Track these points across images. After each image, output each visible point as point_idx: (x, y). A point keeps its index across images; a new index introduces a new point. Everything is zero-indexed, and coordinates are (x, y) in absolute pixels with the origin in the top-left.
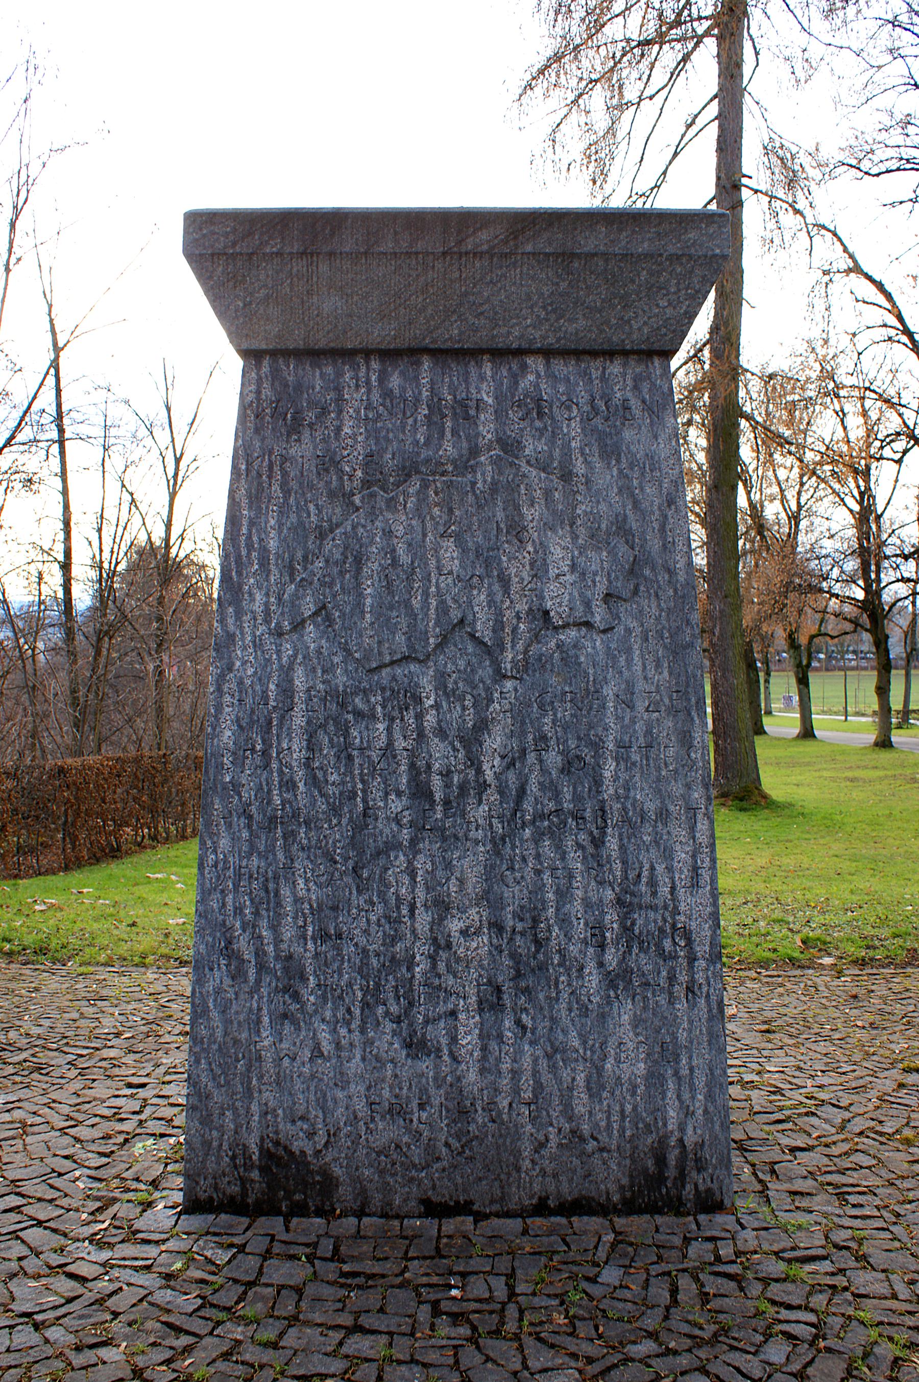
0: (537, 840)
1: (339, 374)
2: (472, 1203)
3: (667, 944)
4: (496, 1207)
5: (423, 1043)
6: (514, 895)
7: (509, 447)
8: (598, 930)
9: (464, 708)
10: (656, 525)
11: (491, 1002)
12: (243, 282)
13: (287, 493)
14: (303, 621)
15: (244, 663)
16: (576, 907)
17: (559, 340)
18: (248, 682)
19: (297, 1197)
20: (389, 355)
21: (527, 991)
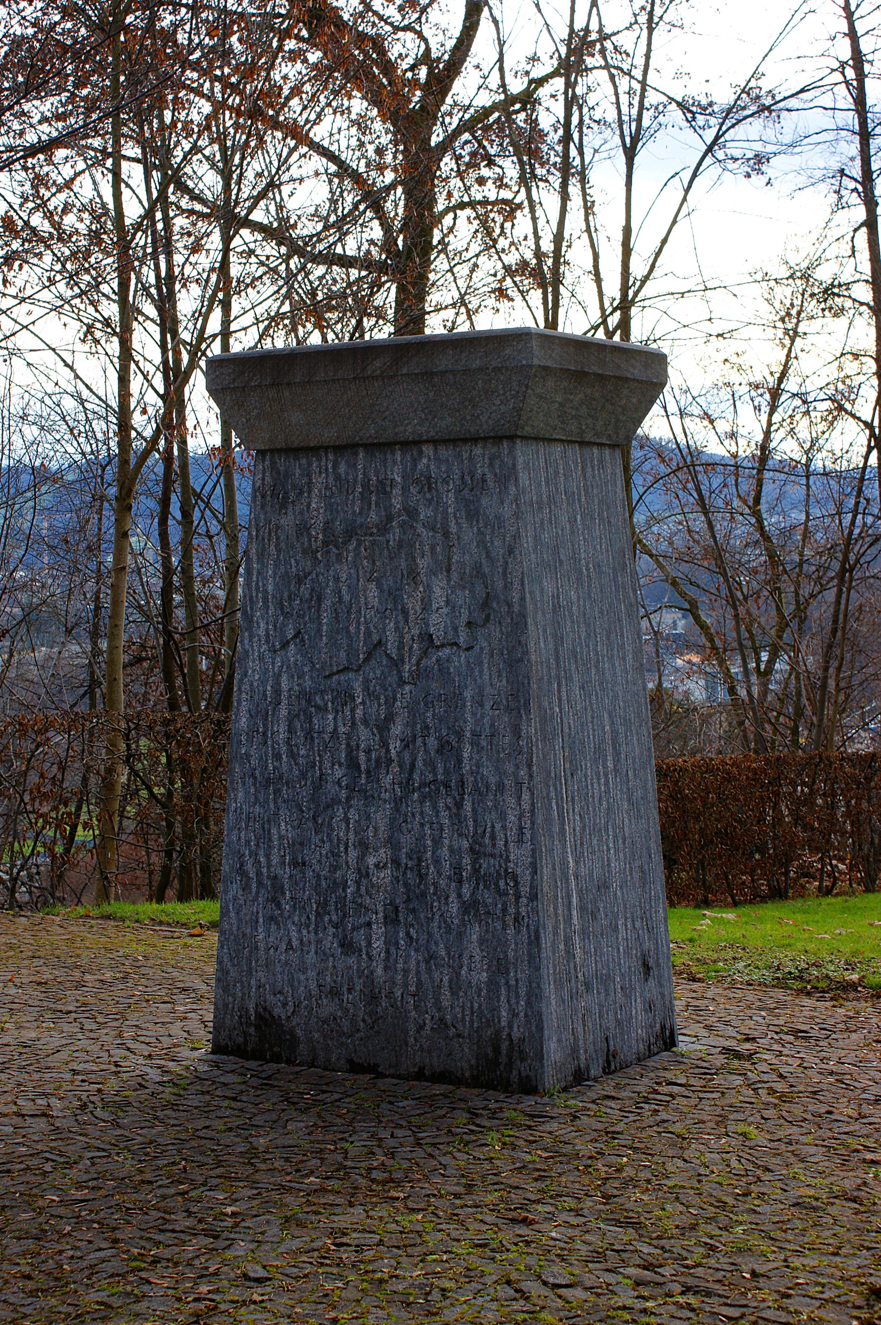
0: (422, 802)
1: (310, 464)
2: (377, 1065)
3: (502, 883)
4: (392, 1071)
5: (351, 944)
6: (407, 841)
7: (412, 513)
8: (458, 869)
9: (379, 705)
10: (500, 570)
11: (392, 919)
12: (243, 405)
13: (279, 551)
14: (288, 642)
15: (254, 671)
16: (445, 852)
17: (437, 433)
18: (255, 684)
19: (276, 1049)
20: (339, 449)
21: (413, 911)
